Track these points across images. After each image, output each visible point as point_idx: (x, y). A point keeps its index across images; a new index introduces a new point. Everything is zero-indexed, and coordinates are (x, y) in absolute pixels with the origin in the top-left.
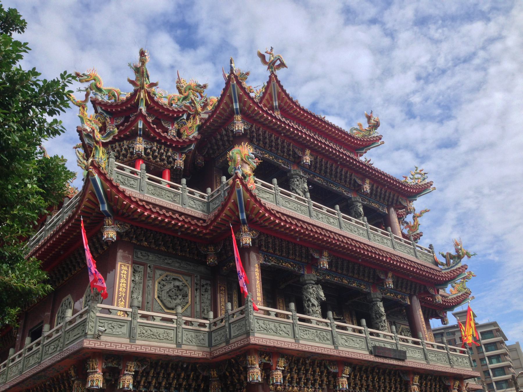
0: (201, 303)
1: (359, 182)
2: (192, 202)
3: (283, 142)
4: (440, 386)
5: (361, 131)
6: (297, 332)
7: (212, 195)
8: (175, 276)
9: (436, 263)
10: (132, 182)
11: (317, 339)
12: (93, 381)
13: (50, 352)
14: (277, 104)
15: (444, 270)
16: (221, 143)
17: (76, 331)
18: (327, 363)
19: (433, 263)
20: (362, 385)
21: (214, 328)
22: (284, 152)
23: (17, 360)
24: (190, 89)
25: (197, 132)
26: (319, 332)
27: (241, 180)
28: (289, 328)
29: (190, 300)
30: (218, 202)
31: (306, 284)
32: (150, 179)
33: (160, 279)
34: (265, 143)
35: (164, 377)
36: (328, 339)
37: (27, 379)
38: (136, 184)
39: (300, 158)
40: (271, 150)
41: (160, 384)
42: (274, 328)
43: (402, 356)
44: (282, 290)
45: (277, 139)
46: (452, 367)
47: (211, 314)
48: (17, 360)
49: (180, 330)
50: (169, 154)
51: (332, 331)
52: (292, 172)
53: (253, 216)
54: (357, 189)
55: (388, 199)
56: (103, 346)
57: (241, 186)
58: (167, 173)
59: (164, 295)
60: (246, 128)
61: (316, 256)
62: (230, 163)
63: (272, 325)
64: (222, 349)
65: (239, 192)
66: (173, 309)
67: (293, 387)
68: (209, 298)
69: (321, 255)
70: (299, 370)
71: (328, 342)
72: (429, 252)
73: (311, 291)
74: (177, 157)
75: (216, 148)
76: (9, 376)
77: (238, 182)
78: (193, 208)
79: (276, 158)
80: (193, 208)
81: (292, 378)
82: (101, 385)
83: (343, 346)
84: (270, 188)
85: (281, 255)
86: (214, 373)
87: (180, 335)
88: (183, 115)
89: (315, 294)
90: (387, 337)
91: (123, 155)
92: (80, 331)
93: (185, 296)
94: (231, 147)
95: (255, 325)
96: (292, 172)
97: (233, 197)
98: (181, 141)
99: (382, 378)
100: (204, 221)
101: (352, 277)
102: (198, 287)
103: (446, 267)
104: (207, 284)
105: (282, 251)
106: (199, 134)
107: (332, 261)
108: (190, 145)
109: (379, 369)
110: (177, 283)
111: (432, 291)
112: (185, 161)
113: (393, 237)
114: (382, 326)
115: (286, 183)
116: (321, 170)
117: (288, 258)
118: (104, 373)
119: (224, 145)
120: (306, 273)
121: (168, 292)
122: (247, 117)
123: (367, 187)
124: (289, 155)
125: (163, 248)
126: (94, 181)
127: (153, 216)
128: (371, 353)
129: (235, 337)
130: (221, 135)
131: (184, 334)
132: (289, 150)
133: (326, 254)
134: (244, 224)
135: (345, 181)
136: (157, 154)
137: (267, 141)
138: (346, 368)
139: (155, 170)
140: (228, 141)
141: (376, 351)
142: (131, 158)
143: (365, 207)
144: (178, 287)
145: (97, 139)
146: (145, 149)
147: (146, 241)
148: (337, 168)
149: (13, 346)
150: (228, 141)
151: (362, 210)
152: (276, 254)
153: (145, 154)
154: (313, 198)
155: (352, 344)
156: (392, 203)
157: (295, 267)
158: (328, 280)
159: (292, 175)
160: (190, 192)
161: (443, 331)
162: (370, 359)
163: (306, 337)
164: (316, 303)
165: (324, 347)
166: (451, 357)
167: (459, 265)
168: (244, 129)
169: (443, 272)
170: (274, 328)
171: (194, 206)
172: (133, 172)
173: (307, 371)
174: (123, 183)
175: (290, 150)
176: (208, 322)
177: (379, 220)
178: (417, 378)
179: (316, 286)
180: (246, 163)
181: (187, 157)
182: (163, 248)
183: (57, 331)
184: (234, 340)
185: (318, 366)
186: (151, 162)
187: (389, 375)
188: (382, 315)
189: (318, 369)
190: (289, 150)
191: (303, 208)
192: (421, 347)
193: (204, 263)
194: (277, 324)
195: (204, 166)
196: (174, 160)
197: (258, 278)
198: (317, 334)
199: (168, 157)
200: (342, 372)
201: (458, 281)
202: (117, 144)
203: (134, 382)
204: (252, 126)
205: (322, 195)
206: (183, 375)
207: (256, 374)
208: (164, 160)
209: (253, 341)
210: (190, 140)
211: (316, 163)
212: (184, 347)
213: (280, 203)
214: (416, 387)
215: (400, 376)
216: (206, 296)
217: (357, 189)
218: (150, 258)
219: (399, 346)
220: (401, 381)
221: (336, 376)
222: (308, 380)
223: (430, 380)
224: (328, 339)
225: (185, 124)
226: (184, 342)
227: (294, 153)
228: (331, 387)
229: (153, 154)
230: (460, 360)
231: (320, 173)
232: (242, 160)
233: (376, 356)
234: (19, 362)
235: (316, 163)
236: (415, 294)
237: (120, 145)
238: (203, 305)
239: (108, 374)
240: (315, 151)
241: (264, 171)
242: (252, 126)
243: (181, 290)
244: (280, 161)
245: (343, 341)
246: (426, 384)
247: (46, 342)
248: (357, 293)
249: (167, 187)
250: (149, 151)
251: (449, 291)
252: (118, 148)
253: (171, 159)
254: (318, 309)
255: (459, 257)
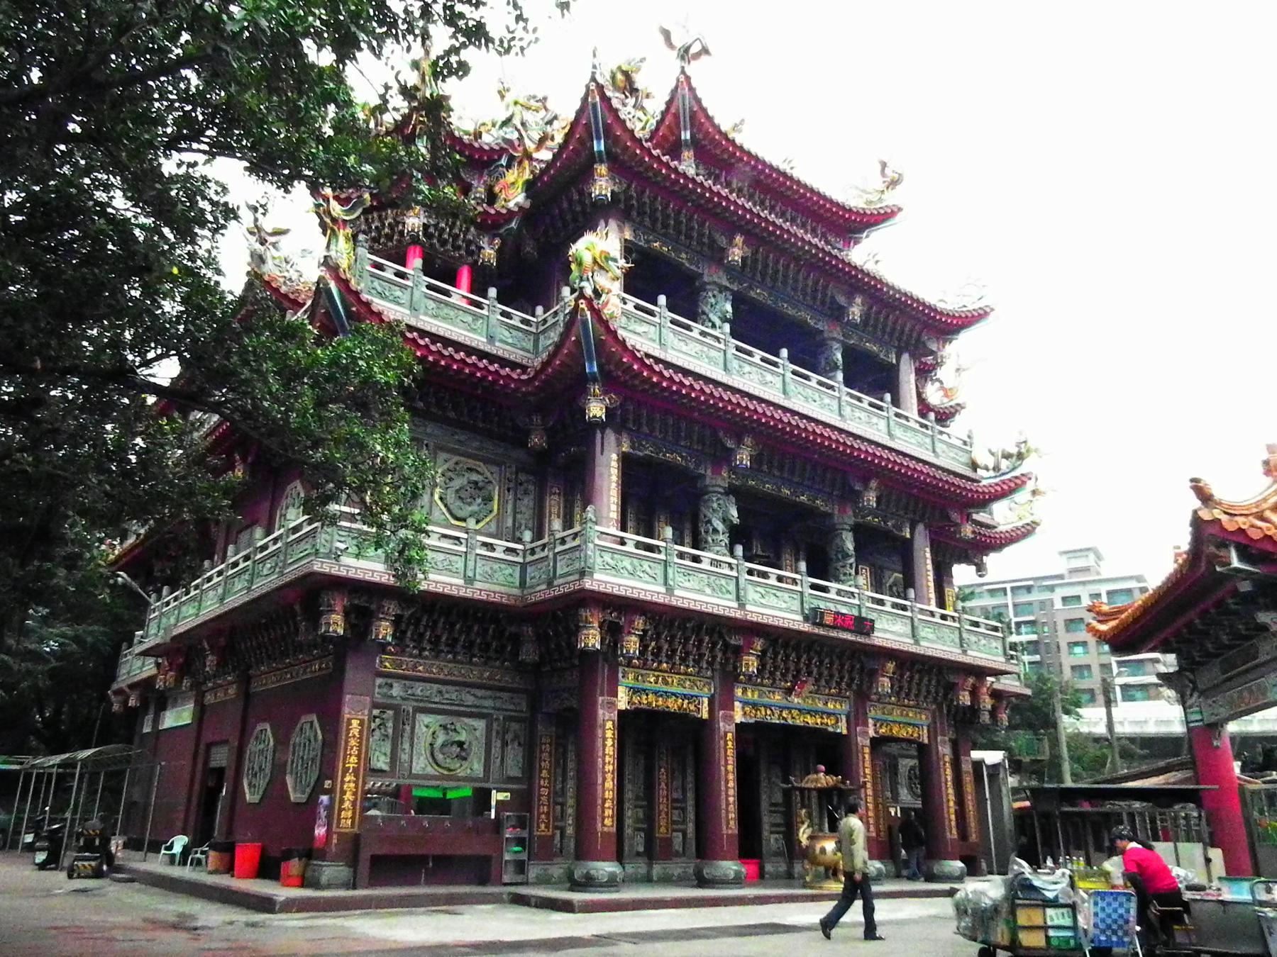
0: (515, 513)
1: (841, 300)
2: (507, 333)
3: (690, 219)
4: (938, 682)
5: (864, 191)
6: (670, 575)
7: (545, 321)
8: (471, 463)
9: (974, 466)
10: (398, 293)
11: (708, 591)
12: (328, 624)
13: (265, 572)
14: (688, 137)
15: (987, 479)
16: (569, 217)
17: (303, 546)
18: (724, 631)
19: (967, 465)
20: (787, 669)
21: (529, 558)
22: (691, 238)
23: (216, 580)
24: (516, 103)
25: (524, 194)
26: (713, 578)
27: (589, 301)
28: (659, 570)
29: (496, 507)
30: (554, 336)
31: (707, 493)
32: (430, 287)
33: (445, 467)
34: (654, 221)
35: (444, 628)
36: (728, 592)
37: (205, 623)
38: (405, 297)
39: (723, 251)
40: (665, 235)
41: (438, 638)
42: (629, 567)
43: (863, 625)
44: (660, 501)
45: (679, 212)
46: (965, 652)
47: (527, 536)
48: (216, 580)
49: (471, 557)
50: (470, 237)
51: (737, 578)
52: (706, 279)
53: (612, 367)
54: (836, 313)
55: (895, 339)
56: (343, 573)
57: (588, 313)
58: (465, 279)
59: (451, 497)
60: (616, 189)
61: (730, 444)
62: (573, 266)
63: (627, 563)
64: (541, 592)
65: (585, 323)
66: (464, 520)
67: (660, 663)
68: (531, 504)
69: (739, 441)
70: (673, 637)
71: (728, 596)
72: (965, 443)
73: (715, 505)
74: (484, 242)
75: (578, 209)
76: (203, 604)
77: (583, 306)
78: (507, 344)
79: (674, 250)
80: (507, 344)
81: (659, 649)
82: (340, 631)
83: (755, 603)
84: (651, 313)
85: (664, 439)
86: (529, 630)
87: (471, 564)
88: (500, 158)
89: (723, 513)
90: (850, 594)
91: (386, 235)
92: (308, 546)
93: (487, 500)
94: (576, 235)
95: (597, 560)
96: (706, 279)
97: (574, 330)
98: (493, 212)
99: (827, 661)
100: (524, 368)
101: (801, 484)
102: (512, 485)
103: (992, 473)
104: (528, 481)
105: (667, 432)
106: (527, 197)
107: (760, 455)
108: (509, 221)
109: (822, 645)
110: (475, 477)
111: (955, 516)
112: (499, 252)
113: (891, 414)
114: (845, 574)
115: (687, 306)
116: (764, 275)
117: (677, 444)
118: (347, 614)
119: (575, 220)
120: (709, 472)
121: (457, 491)
122: (620, 164)
123: (856, 312)
124: (702, 244)
125: (452, 415)
126: (329, 292)
127: (431, 358)
128: (806, 619)
129: (562, 576)
130: (570, 201)
131: (479, 565)
132: (701, 235)
133: (748, 440)
134: (595, 380)
135: (814, 298)
136: (446, 236)
137: (659, 215)
138: (756, 639)
139: (442, 271)
140: (584, 212)
141: (814, 616)
142: (399, 241)
143: (848, 352)
144: (476, 483)
145: (334, 214)
146: (426, 227)
147: (421, 399)
148: (799, 271)
149: (211, 558)
150: (584, 212)
151: (839, 356)
152: (656, 437)
153: (425, 235)
154: (734, 334)
155: (772, 601)
156: (907, 343)
157: (690, 463)
158: (752, 487)
159: (706, 283)
160: (504, 314)
161: (1031, 583)
162: (801, 628)
163: (687, 584)
164: (720, 526)
165: (719, 603)
166: (965, 635)
167: (1017, 473)
168: (613, 192)
169: (984, 482)
170: (629, 567)
171: (510, 341)
172: (399, 274)
173: (687, 639)
174: (381, 295)
175: (703, 235)
176: (520, 547)
177: (872, 378)
178: (891, 666)
179: (724, 497)
180: (601, 268)
181: (503, 244)
182: (452, 415)
183: (275, 541)
184: (561, 581)
185: (707, 634)
186: (436, 250)
187: (840, 658)
188: (847, 556)
189: (707, 639)
190: (701, 235)
191: (713, 353)
192: (908, 614)
193: (523, 444)
194: (635, 561)
195: (528, 271)
196: (480, 248)
197: (614, 478)
198: (711, 582)
199: (469, 243)
200: (750, 645)
201: (1022, 496)
202: (375, 215)
203: (395, 631)
204: (629, 186)
205: (757, 328)
206: (476, 628)
207: (592, 639)
208: (459, 248)
209: (588, 584)
210: (509, 210)
211: (755, 261)
212: (478, 585)
213: (669, 344)
214: (887, 680)
215: (860, 661)
216: (526, 502)
217: (837, 314)
218: (429, 430)
219: (863, 610)
220: (862, 668)
221: (738, 652)
222: (688, 654)
223: (919, 672)
224: (728, 592)
225: (503, 175)
226: (478, 577)
227: (713, 241)
228: (730, 668)
229: (440, 235)
230: (983, 642)
231: (763, 280)
232: (595, 261)
233: (814, 624)
234: (218, 584)
235: (755, 261)
236: (921, 520)
237: (380, 217)
238: (519, 516)
239: (353, 616)
240: (756, 235)
241: (645, 278)
242: (629, 186)
243: (480, 489)
244: (684, 256)
245: (757, 597)
246: (912, 678)
247: (259, 556)
248: (807, 512)
249: (464, 304)
250: (432, 230)
251: (1002, 515)
252: (377, 223)
253: (473, 248)
254: (725, 539)
255: (1020, 456)
